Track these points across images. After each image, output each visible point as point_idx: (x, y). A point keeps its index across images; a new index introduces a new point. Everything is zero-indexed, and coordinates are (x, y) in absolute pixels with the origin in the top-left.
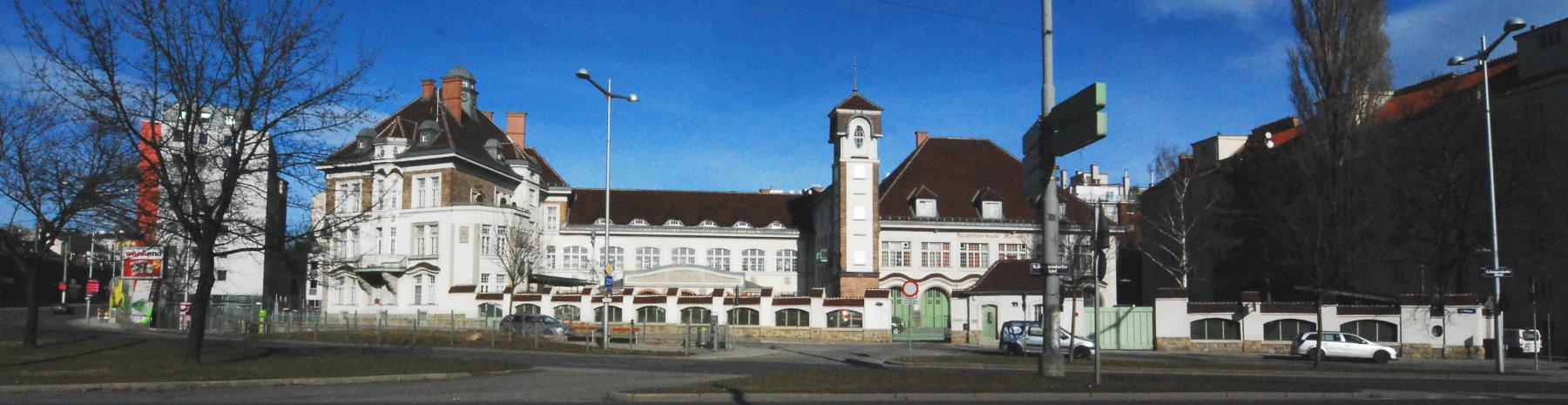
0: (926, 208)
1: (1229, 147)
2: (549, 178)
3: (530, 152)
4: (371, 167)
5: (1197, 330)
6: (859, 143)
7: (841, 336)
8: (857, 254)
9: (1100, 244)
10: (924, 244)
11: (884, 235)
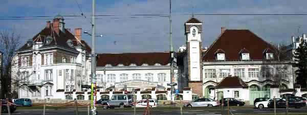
2: (88, 50)
3: (83, 42)
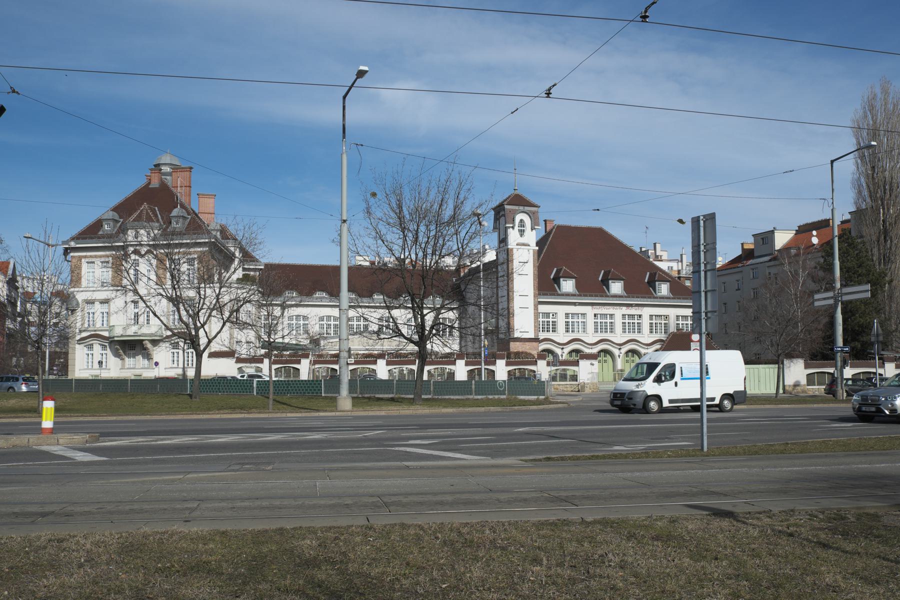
0: (568, 285)
1: (781, 240)
4: (124, 248)
5: (810, 379)
6: (522, 233)
7: (561, 388)
8: (523, 323)
9: (480, 310)
10: (567, 315)
11: (543, 308)
